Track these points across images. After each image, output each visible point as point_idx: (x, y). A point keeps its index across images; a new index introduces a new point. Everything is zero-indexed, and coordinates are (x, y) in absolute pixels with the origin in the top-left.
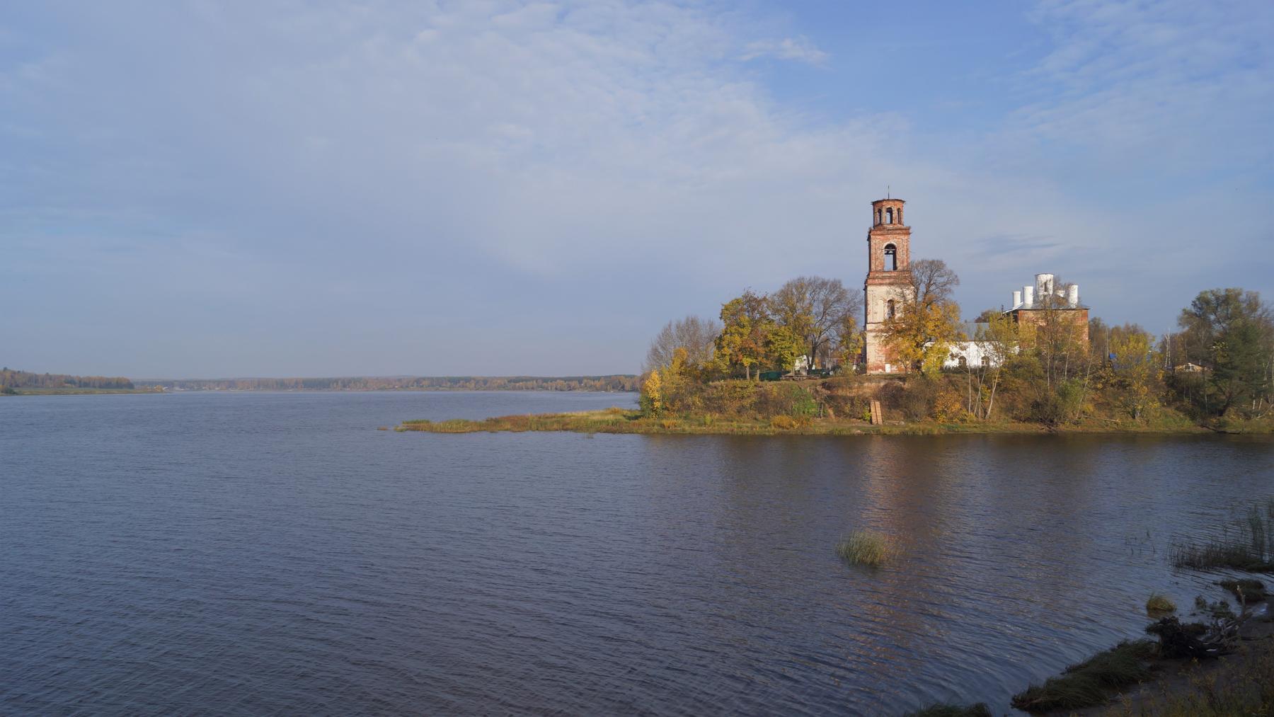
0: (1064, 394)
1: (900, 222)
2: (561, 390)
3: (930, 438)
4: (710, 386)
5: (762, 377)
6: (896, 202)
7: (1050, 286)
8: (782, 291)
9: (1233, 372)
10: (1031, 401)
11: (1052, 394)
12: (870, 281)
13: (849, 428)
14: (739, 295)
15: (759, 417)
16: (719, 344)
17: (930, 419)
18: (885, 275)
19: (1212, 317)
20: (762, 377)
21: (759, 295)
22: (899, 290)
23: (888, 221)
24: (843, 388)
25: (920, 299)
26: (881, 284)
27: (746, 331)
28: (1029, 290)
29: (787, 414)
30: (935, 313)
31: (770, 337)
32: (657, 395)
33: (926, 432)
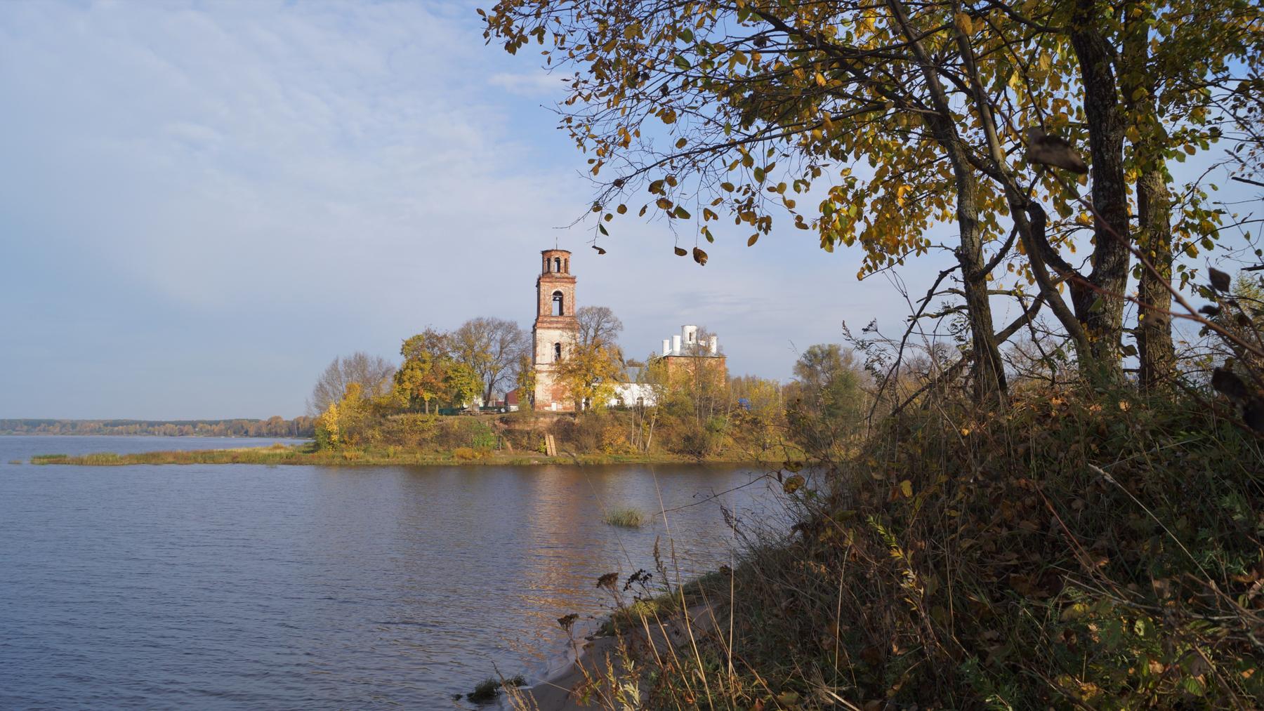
0: (710, 429)
1: (566, 271)
2: (171, 435)
3: (599, 468)
4: (388, 420)
5: (441, 412)
6: (564, 253)
7: (694, 336)
8: (462, 330)
9: (838, 411)
10: (683, 435)
11: (701, 429)
12: (539, 325)
13: (528, 459)
14: (420, 331)
15: (440, 449)
16: (400, 378)
17: (598, 451)
18: (552, 319)
19: (819, 368)
20: (441, 412)
21: (440, 333)
22: (570, 333)
23: (556, 270)
24: (519, 423)
25: (589, 342)
26: (549, 328)
27: (427, 366)
28: (677, 339)
29: (468, 446)
30: (603, 355)
31: (450, 373)
32: (335, 428)
33: (597, 462)
